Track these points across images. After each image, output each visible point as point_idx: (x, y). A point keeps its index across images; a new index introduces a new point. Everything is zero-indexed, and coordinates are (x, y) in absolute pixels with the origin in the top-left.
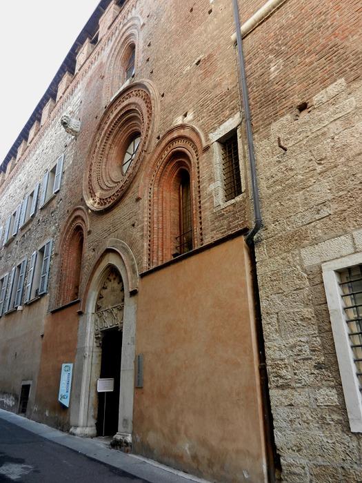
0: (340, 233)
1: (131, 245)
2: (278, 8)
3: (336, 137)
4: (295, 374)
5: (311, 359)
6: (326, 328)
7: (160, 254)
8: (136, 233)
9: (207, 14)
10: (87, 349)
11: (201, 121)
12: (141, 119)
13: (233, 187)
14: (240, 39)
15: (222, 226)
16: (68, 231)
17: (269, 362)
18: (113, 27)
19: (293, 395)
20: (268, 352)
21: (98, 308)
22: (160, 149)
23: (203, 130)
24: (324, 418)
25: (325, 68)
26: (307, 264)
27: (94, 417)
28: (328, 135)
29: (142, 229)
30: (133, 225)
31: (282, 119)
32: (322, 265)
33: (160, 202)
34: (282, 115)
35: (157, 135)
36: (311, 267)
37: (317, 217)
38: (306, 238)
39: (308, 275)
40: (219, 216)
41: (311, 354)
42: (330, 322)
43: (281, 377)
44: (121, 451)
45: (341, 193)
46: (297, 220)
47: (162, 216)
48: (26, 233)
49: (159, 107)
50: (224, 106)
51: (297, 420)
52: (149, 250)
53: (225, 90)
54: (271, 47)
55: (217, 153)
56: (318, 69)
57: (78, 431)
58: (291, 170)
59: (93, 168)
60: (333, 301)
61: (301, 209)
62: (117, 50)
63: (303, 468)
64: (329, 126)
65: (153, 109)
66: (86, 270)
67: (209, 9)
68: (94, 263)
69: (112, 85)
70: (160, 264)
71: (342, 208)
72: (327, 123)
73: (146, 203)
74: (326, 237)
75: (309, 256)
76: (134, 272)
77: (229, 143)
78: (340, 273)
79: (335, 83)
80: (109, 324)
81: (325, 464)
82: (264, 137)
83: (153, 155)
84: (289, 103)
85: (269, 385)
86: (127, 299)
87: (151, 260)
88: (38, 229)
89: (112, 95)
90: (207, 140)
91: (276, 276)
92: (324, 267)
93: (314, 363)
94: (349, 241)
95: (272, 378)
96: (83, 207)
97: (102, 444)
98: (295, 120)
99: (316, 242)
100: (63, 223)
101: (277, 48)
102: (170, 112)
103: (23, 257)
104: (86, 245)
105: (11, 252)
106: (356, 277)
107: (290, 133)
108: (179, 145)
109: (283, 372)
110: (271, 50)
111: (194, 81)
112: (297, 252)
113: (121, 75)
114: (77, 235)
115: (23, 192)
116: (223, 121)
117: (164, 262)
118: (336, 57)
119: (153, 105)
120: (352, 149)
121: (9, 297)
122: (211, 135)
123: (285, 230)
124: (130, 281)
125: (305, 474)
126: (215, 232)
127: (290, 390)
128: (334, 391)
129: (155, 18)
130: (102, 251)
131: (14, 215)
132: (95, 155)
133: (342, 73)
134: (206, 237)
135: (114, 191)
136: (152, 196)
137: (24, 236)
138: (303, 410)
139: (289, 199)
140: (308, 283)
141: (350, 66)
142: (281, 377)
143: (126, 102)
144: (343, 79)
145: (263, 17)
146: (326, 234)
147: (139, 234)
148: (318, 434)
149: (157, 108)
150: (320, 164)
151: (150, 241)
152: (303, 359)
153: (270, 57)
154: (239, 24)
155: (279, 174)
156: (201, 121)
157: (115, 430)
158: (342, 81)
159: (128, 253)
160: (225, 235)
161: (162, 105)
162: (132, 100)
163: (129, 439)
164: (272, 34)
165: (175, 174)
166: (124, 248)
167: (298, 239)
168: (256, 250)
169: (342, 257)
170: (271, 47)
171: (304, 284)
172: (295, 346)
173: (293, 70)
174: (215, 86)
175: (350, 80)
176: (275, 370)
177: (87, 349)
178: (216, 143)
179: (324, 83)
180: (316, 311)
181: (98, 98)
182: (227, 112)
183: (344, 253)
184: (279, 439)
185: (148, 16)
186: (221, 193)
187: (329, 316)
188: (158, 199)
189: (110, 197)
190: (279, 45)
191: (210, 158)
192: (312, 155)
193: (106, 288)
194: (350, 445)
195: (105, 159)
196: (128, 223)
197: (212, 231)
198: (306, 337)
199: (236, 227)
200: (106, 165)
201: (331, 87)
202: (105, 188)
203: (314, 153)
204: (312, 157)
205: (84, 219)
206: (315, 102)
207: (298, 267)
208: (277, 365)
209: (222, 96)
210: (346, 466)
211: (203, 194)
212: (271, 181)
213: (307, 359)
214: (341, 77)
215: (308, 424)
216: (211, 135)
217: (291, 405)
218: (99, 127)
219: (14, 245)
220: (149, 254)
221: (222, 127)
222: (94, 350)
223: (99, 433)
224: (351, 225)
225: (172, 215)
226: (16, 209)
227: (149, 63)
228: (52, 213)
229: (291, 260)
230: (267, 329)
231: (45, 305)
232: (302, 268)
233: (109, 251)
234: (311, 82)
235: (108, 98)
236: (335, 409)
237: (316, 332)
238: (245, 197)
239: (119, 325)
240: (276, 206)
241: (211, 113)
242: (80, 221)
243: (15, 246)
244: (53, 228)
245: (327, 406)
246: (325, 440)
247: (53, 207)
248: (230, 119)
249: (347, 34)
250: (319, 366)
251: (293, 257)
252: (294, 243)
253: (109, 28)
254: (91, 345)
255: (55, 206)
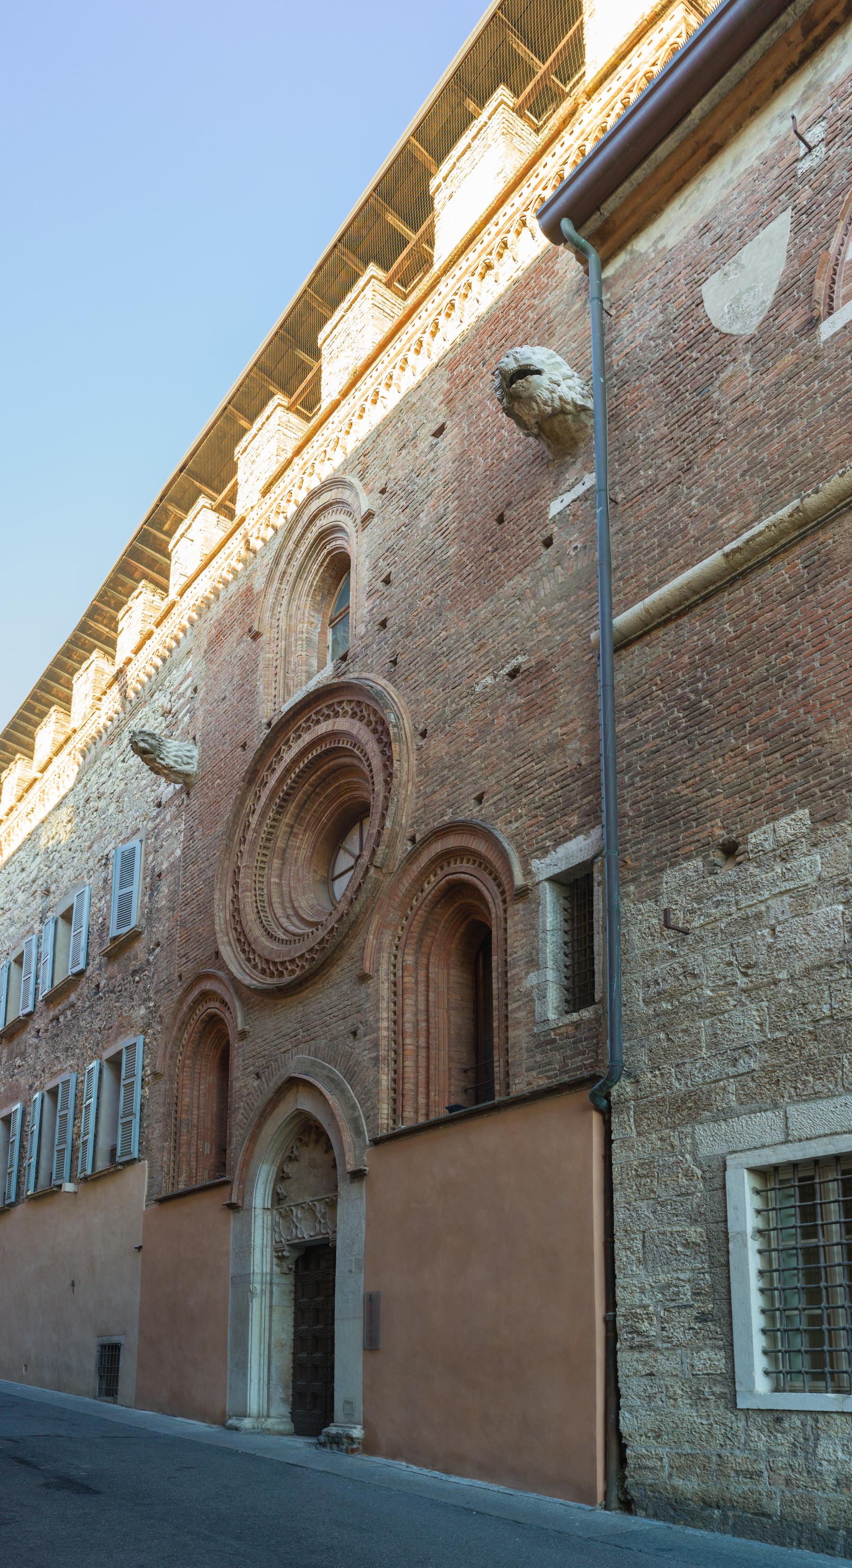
0: (767, 1106)
1: (351, 1075)
2: (705, 599)
3: (779, 928)
4: (663, 1329)
5: (691, 1306)
6: (722, 1260)
7: (422, 1100)
8: (362, 1053)
9: (540, 548)
10: (258, 1278)
11: (515, 825)
12: (366, 770)
13: (580, 988)
14: (609, 649)
15: (549, 1064)
16: (184, 1024)
17: (620, 1310)
18: (277, 490)
19: (656, 1361)
20: (619, 1293)
21: (278, 1199)
22: (416, 869)
23: (518, 847)
24: (699, 1391)
25: (779, 777)
26: (704, 1151)
27: (284, 1400)
28: (765, 922)
29: (376, 1044)
30: (354, 1034)
31: (685, 865)
32: (728, 1157)
33: (422, 988)
34: (688, 858)
35: (410, 832)
36: (710, 1158)
37: (731, 1071)
38: (708, 1107)
39: (704, 1172)
40: (544, 1042)
41: (694, 1300)
42: (728, 1252)
43: (639, 1333)
44: (341, 1451)
45: (778, 1034)
46: (696, 1073)
47: (427, 1021)
48: (63, 1012)
49: (414, 762)
50: (569, 802)
51: (658, 1396)
52: (395, 1090)
53: (571, 763)
54: (679, 691)
55: (550, 913)
56: (766, 775)
57: (247, 1423)
58: (694, 976)
59: (241, 882)
60: (737, 1218)
61: (704, 1053)
62: (296, 564)
63: (661, 1459)
64: (770, 902)
65: (396, 764)
66: (240, 1118)
67: (546, 534)
68: (259, 1103)
69: (287, 662)
70: (422, 1120)
71: (775, 1062)
72: (767, 894)
73: (385, 989)
74: (742, 1109)
75: (709, 1139)
76: (358, 1132)
77: (576, 886)
78: (761, 1173)
79: (793, 816)
80: (306, 1232)
81: (694, 1452)
82: (648, 896)
83: (399, 881)
84: (702, 835)
85: (618, 1345)
86: (344, 1188)
87: (399, 1112)
88: (98, 1009)
89: (288, 692)
90: (527, 873)
91: (647, 1169)
92: (731, 1161)
93: (695, 1313)
94: (779, 1122)
95: (623, 1335)
96: (221, 974)
97: (300, 1448)
98: (711, 874)
99: (725, 1115)
100: (167, 1004)
101: (692, 697)
102: (442, 783)
103: (62, 1070)
104: (237, 1062)
105: (23, 1055)
106: (794, 1185)
107: (699, 899)
108: (464, 870)
109: (644, 1326)
110: (681, 698)
111: (502, 720)
112: (690, 1130)
113: (316, 638)
114: (212, 1039)
115: (38, 903)
116: (565, 838)
117: (432, 1118)
118: (802, 759)
119: (396, 757)
120: (801, 957)
121: (33, 1161)
122: (535, 864)
123: (670, 1088)
124: (351, 1152)
125: (662, 1467)
126: (534, 1073)
127: (652, 1353)
128: (722, 1353)
129: (403, 503)
130: (276, 1080)
131: (19, 961)
132: (245, 848)
133: (806, 799)
134: (517, 1081)
135: (302, 948)
136: (399, 973)
137: (57, 1019)
138: (669, 1381)
139: (684, 1031)
140: (701, 1186)
141: (823, 787)
142: (639, 1333)
143: (324, 727)
144: (807, 811)
145: (668, 610)
146: (742, 1103)
147: (367, 1056)
148: (686, 1411)
149: (406, 765)
150: (745, 975)
151: (395, 1072)
152: (678, 1307)
153: (676, 714)
154: (610, 612)
155: (670, 980)
156: (516, 825)
157: (328, 1417)
158: (803, 813)
159: (343, 1091)
160: (555, 1082)
161: (420, 760)
162: (342, 724)
163: (357, 1432)
164: (686, 659)
165: (461, 930)
166: (333, 1080)
167: (692, 1107)
168: (615, 1119)
169: (763, 1146)
170: (679, 691)
171: (696, 1187)
172: (668, 1286)
173: (720, 760)
174: (550, 749)
175: (818, 816)
176: (630, 1322)
177: (258, 1278)
178: (547, 885)
179: (776, 808)
180: (708, 1231)
181: (246, 691)
182: (574, 820)
183: (768, 1140)
184: (627, 1422)
185: (383, 492)
186: (553, 996)
187: (727, 1241)
188: (417, 982)
189: (292, 961)
190: (695, 691)
191: (535, 912)
192: (734, 955)
193: (296, 1159)
194: (735, 1426)
195: (276, 863)
196: (342, 1028)
197: (529, 1070)
198: (686, 1273)
199: (578, 1068)
200: (280, 876)
201: (783, 822)
202: (281, 935)
203: (738, 950)
204: (733, 959)
205: (227, 1000)
206: (750, 847)
207: (688, 1156)
208: (635, 1315)
209: (564, 777)
210: (723, 1452)
211: (513, 990)
212: (653, 990)
213: (685, 1307)
214: (803, 807)
215: (675, 1400)
216: (535, 864)
217: (651, 1374)
218: (253, 776)
219: (28, 1038)
220: (395, 1101)
221: (561, 850)
222: (275, 1280)
223: (300, 1430)
224: (786, 1095)
225: (449, 1020)
226: (23, 947)
227: (388, 634)
228: (135, 973)
229: (676, 1143)
230: (621, 1255)
231: (137, 1184)
232: (695, 1160)
233: (292, 1083)
234: (749, 798)
235: (274, 702)
236: (719, 1378)
237: (706, 1265)
238: (600, 1012)
239: (331, 1236)
240: (659, 1040)
241: (538, 812)
242: (217, 1005)
243: (33, 1041)
244: (143, 1011)
245: (708, 1374)
246: (698, 1421)
247: (136, 958)
248: (581, 837)
249: (828, 713)
250: (702, 1318)
251: (681, 1139)
252: (685, 1113)
253: (265, 492)
254: (267, 1269)
255: (142, 956)
